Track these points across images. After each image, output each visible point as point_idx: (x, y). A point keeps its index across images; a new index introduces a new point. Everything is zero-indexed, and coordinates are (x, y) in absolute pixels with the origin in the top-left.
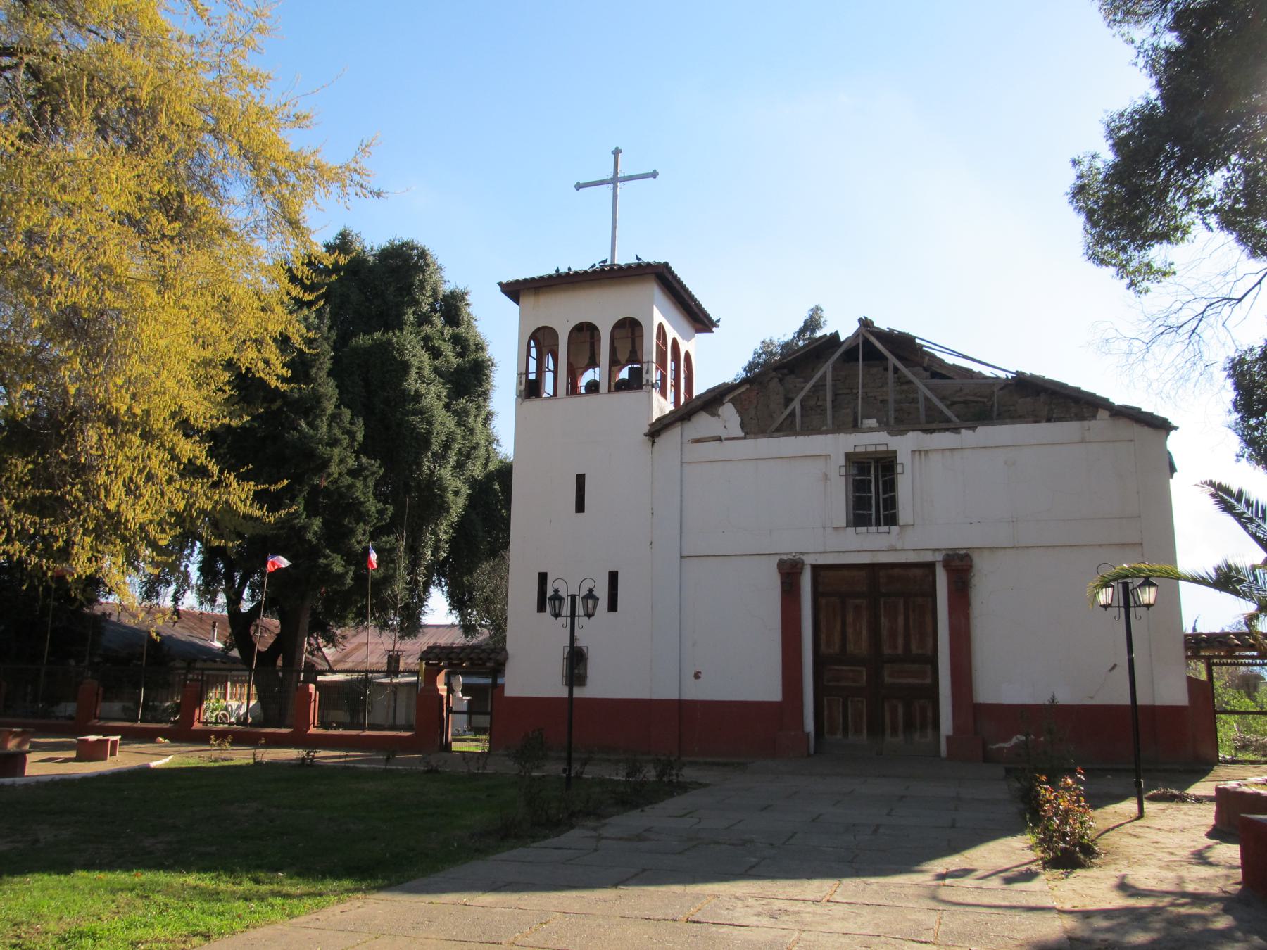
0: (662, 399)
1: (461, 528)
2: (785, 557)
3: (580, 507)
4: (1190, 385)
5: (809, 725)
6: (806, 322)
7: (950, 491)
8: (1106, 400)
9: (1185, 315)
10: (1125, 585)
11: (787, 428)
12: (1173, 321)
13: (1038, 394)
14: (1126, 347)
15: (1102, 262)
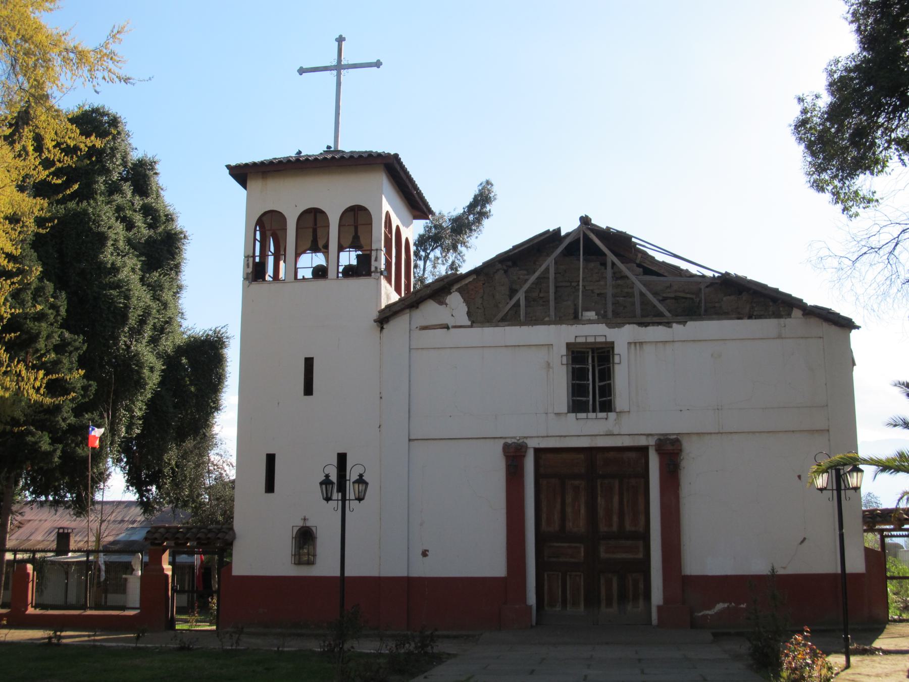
0: (388, 285)
1: (152, 404)
2: (509, 441)
3: (308, 390)
4: (890, 300)
5: (532, 599)
6: (476, 198)
7: (664, 381)
8: (801, 301)
9: (885, 237)
10: (838, 471)
11: (512, 318)
12: (874, 242)
13: (740, 293)
14: (836, 264)
15: (821, 189)
